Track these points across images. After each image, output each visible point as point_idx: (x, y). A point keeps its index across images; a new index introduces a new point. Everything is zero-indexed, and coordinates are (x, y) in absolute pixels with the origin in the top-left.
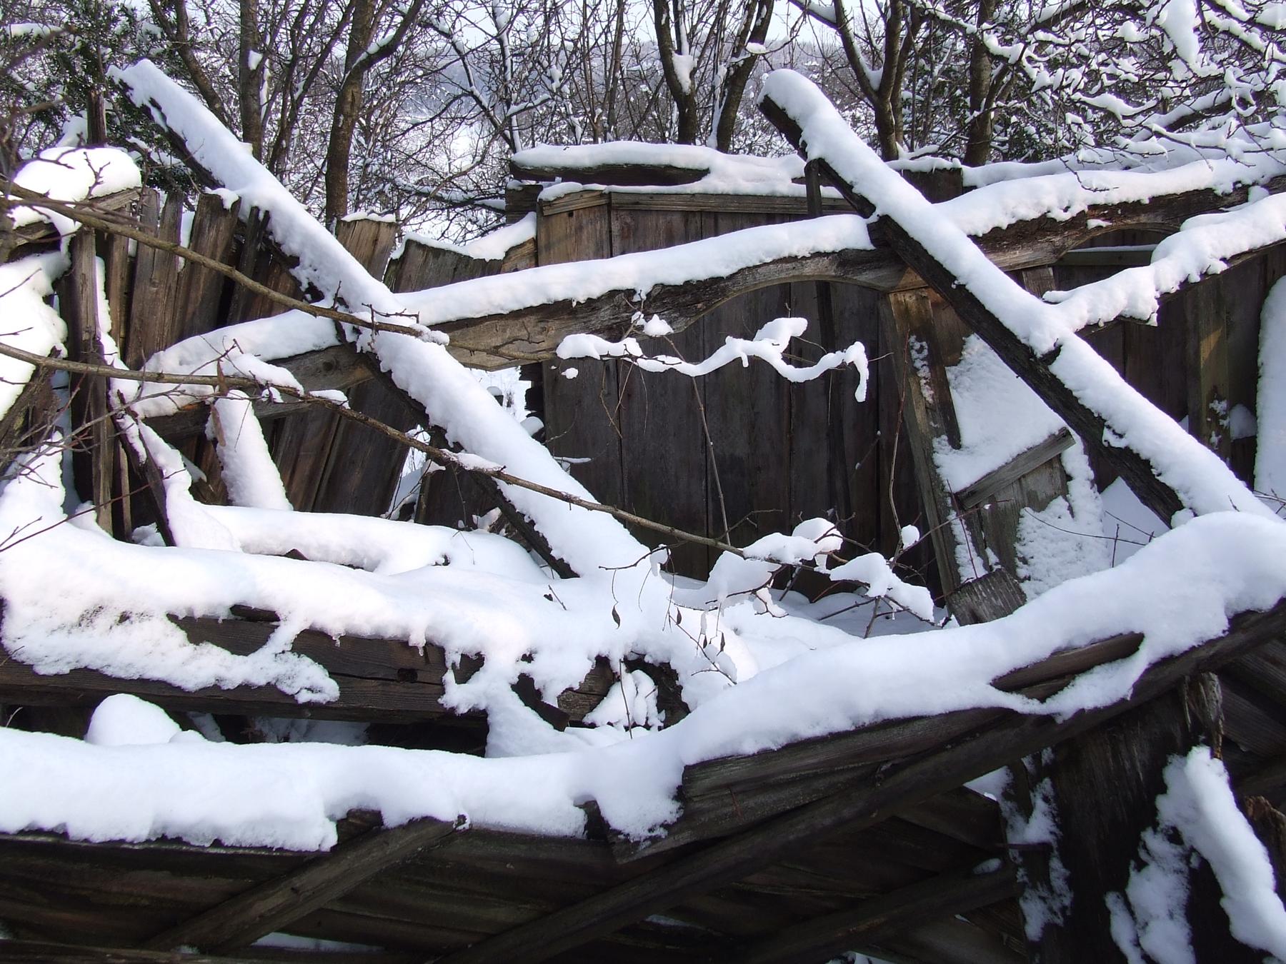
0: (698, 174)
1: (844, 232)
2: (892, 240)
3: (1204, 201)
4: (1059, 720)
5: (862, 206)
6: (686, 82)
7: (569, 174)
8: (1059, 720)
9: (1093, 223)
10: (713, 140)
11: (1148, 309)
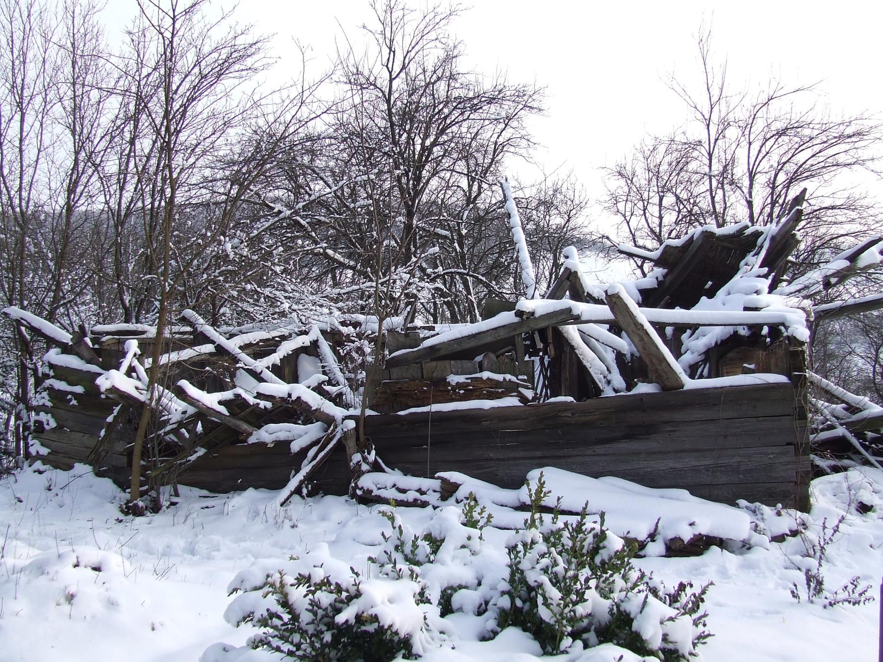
0: (143, 332)
1: (209, 348)
2: (221, 350)
3: (284, 338)
4: (537, 315)
5: (213, 342)
6: (128, 305)
7: (108, 333)
8: (537, 315)
9: (752, 366)
10: (134, 321)
11: (278, 362)
